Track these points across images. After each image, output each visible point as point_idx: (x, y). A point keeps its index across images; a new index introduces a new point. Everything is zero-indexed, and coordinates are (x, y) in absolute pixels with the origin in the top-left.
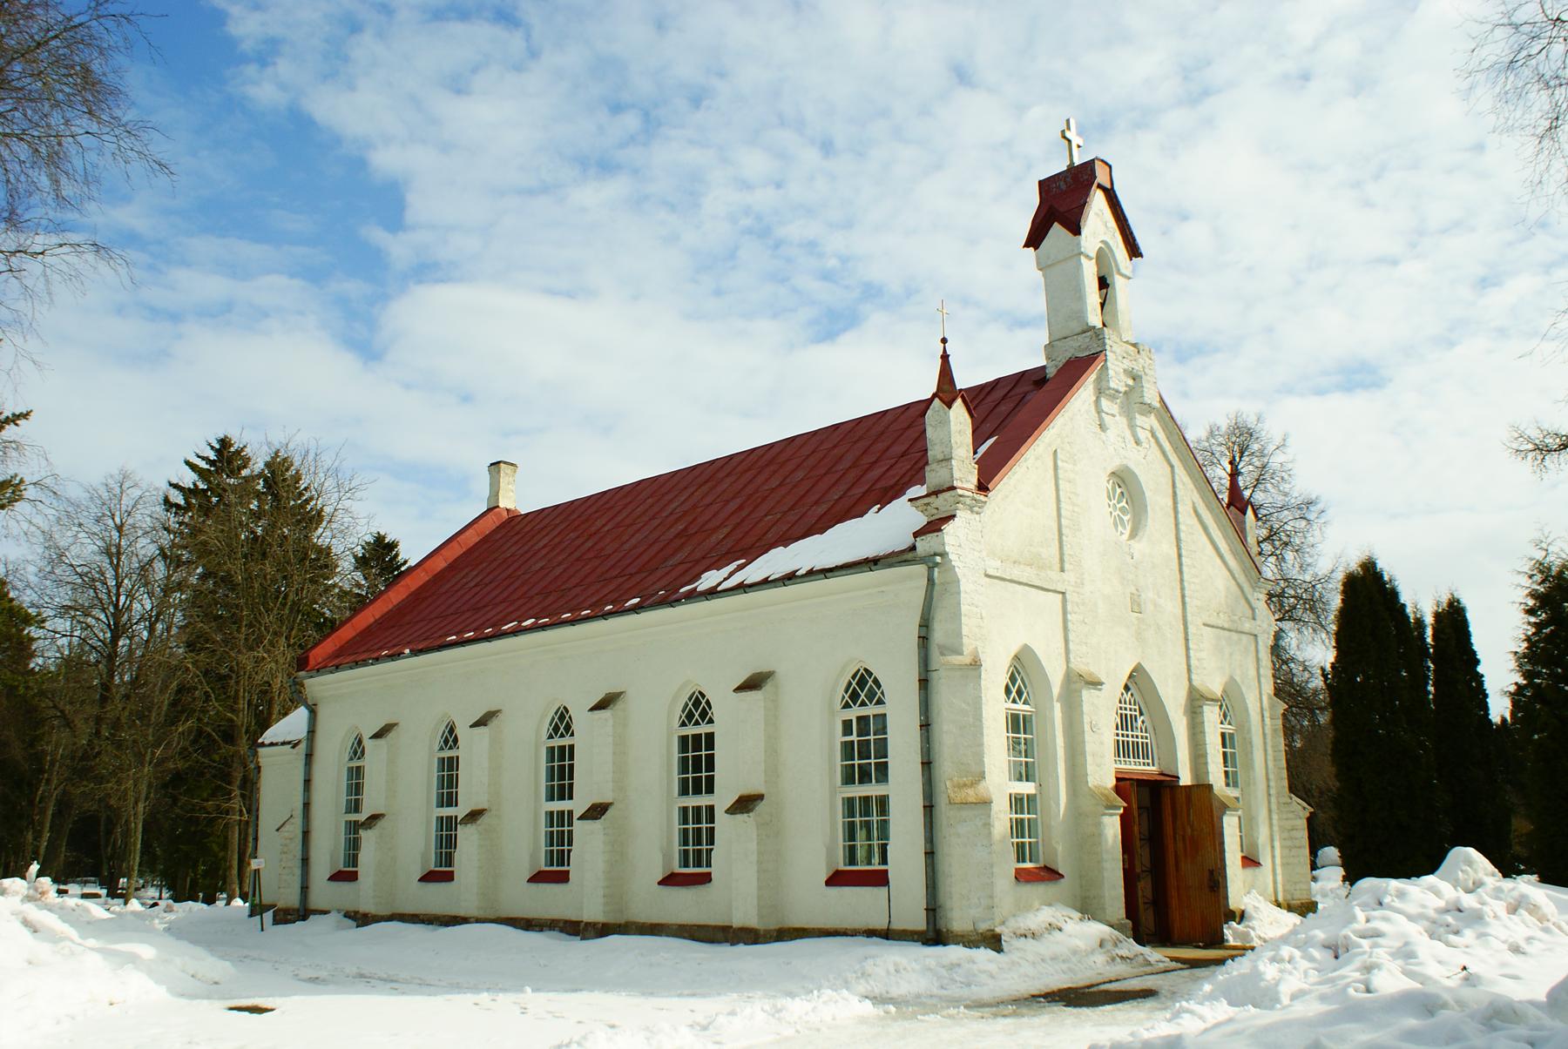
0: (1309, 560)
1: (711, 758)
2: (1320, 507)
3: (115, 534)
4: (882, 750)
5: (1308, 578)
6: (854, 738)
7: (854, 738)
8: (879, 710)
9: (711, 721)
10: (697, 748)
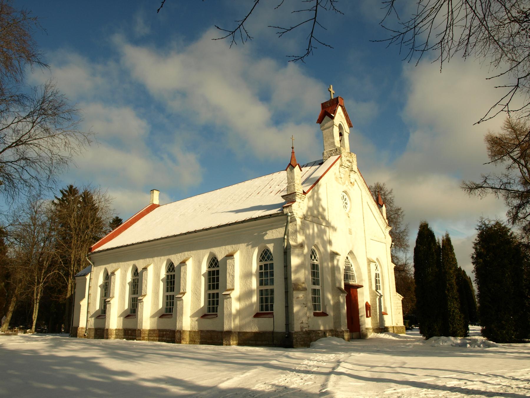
0: (398, 226)
1: (218, 278)
2: (401, 211)
3: (34, 213)
4: (272, 274)
5: (397, 232)
6: (263, 271)
7: (263, 271)
8: (271, 262)
9: (218, 266)
10: (214, 275)
